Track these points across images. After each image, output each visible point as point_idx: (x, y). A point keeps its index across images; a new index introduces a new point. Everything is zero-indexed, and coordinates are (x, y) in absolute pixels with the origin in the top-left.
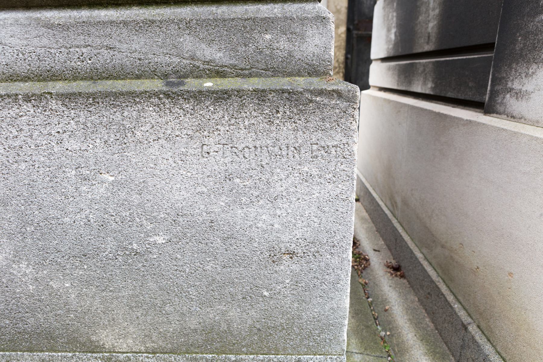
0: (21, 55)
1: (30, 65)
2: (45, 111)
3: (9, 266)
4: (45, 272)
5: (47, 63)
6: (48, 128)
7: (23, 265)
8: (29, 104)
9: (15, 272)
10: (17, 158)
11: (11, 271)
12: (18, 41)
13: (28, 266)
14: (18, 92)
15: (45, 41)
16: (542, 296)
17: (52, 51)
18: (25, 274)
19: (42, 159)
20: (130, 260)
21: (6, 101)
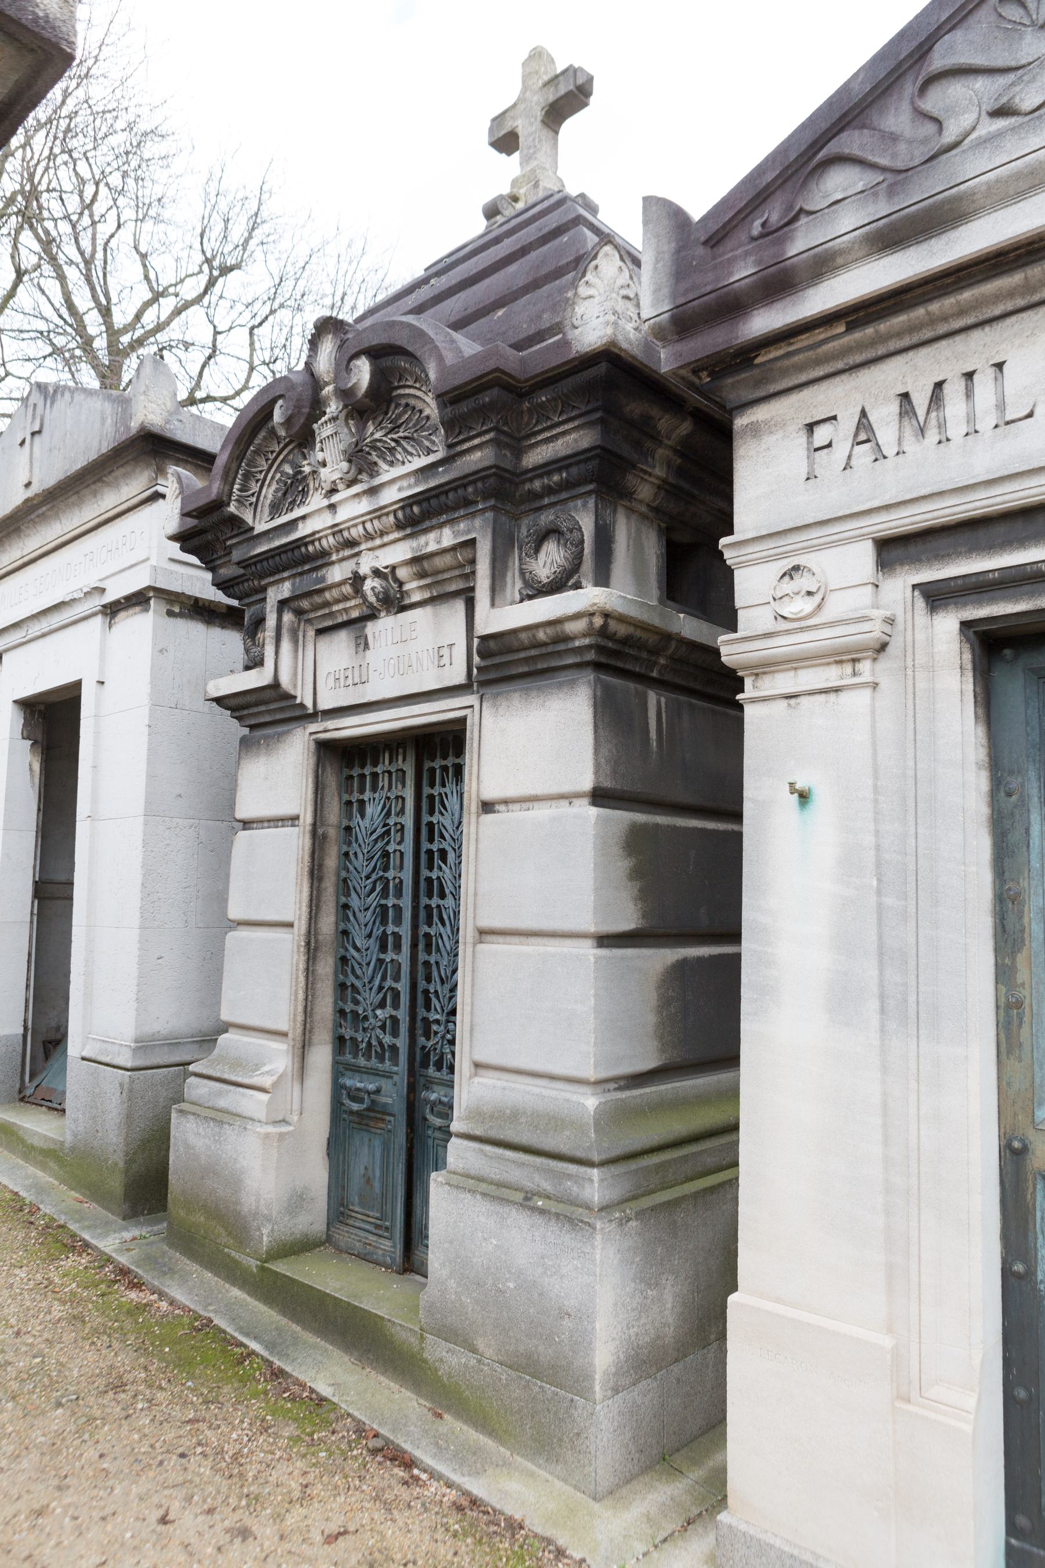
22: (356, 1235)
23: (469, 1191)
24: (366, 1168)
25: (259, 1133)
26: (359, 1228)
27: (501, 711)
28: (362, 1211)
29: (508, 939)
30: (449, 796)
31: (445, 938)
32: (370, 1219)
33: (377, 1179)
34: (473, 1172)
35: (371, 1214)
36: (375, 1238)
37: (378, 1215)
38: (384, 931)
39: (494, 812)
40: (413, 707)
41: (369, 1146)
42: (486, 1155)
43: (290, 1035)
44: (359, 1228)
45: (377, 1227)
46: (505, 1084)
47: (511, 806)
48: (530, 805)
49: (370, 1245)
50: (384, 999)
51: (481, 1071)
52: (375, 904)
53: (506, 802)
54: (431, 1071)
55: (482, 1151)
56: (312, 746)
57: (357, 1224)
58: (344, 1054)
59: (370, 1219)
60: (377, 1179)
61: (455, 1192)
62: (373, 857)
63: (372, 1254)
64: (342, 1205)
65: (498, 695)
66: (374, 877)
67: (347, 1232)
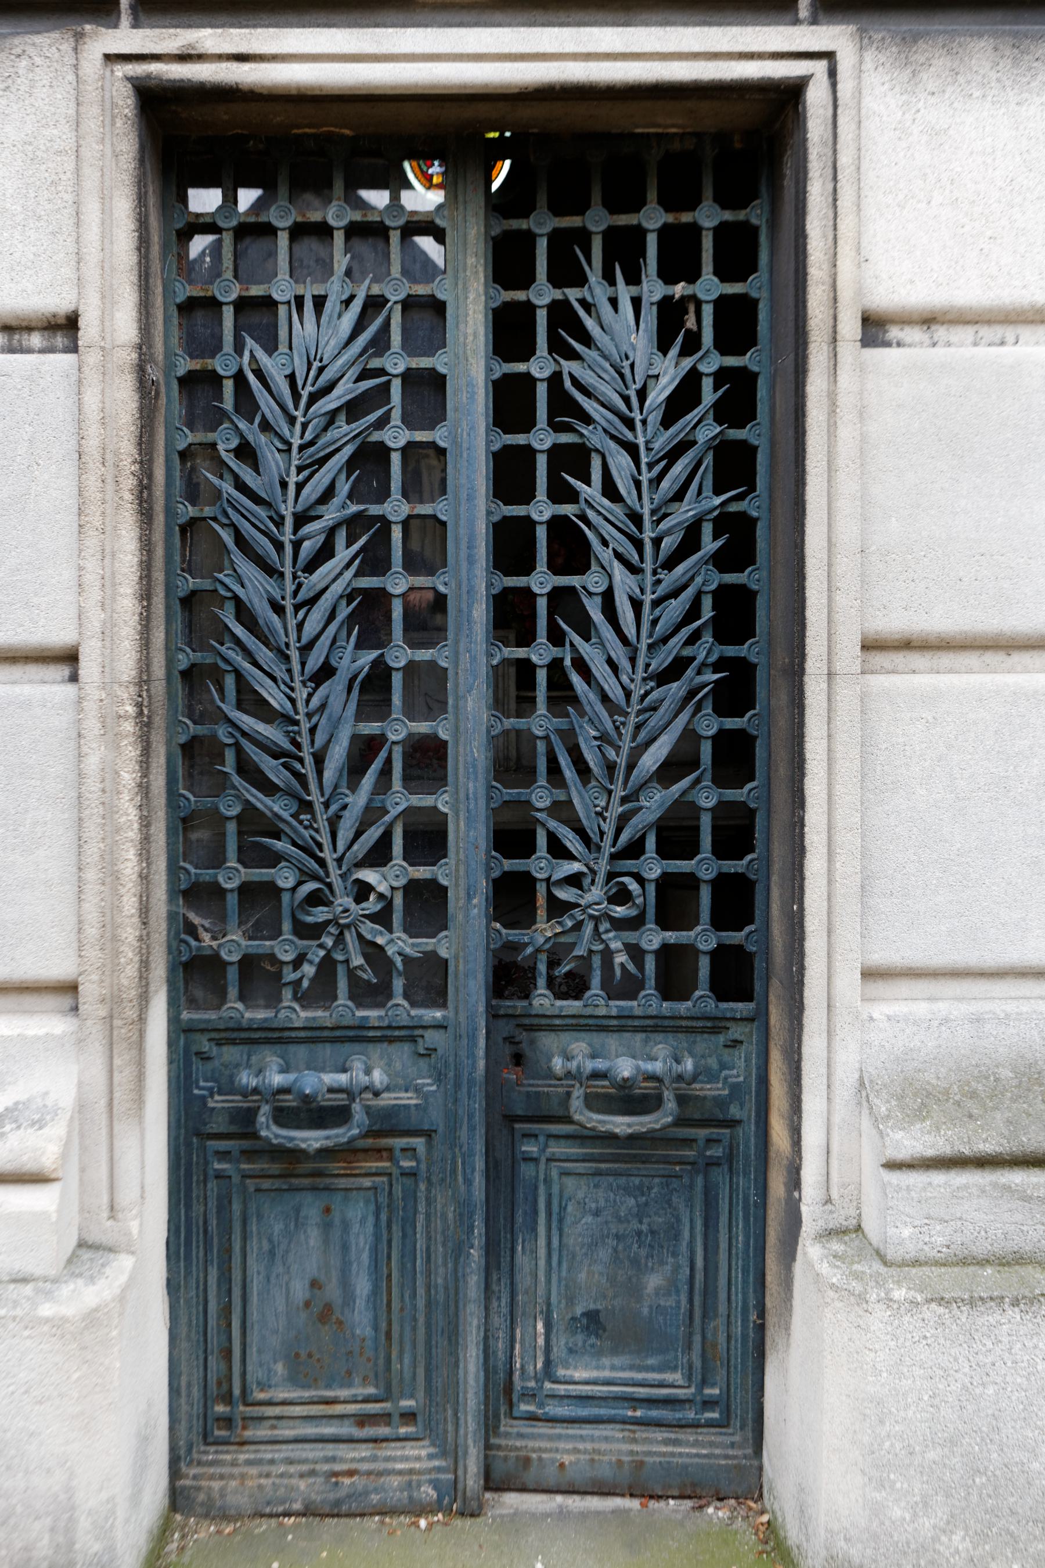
0: (983, 1233)
1: (992, 1245)
2: (1035, 1317)
3: (935, 1539)
4: (987, 1547)
5: (1011, 1246)
6: (1035, 1340)
7: (956, 1538)
8: (1016, 1309)
9: (942, 1549)
10: (984, 1378)
11: (937, 1546)
12: (984, 1216)
13: (964, 1539)
14: (1004, 1293)
15: (1018, 1217)
16: (2, 86)
17: (1025, 1228)
18: (957, 1551)
19: (1019, 1380)
20: (927, 1524)
21: (988, 1305)
22: (290, 1462)
23: (1015, 1303)
24: (314, 1284)
25: (58, 1324)
26: (297, 1441)
27: (929, 79)
28: (307, 1394)
29: (946, 659)
30: (606, 309)
31: (600, 669)
32: (339, 1409)
33: (360, 1303)
34: (981, 1249)
35: (343, 1393)
36: (364, 1451)
37: (371, 1390)
38: (379, 664)
39: (887, 344)
40: (595, 31)
41: (326, 1226)
42: (1027, 1199)
43: (89, 990)
44: (297, 1441)
45: (362, 1420)
46: (974, 1007)
47: (941, 332)
48: (1009, 333)
49: (351, 1473)
50: (386, 839)
51: (880, 988)
52: (338, 588)
53: (929, 320)
54: (543, 1000)
55: (1007, 1188)
56: (126, 102)
57: (289, 1433)
58: (223, 997)
59: (339, 1409)
60: (360, 1303)
61: (964, 1315)
62: (322, 461)
63: (366, 1493)
64: (227, 1398)
65: (916, 38)
66: (331, 514)
67: (249, 1463)
